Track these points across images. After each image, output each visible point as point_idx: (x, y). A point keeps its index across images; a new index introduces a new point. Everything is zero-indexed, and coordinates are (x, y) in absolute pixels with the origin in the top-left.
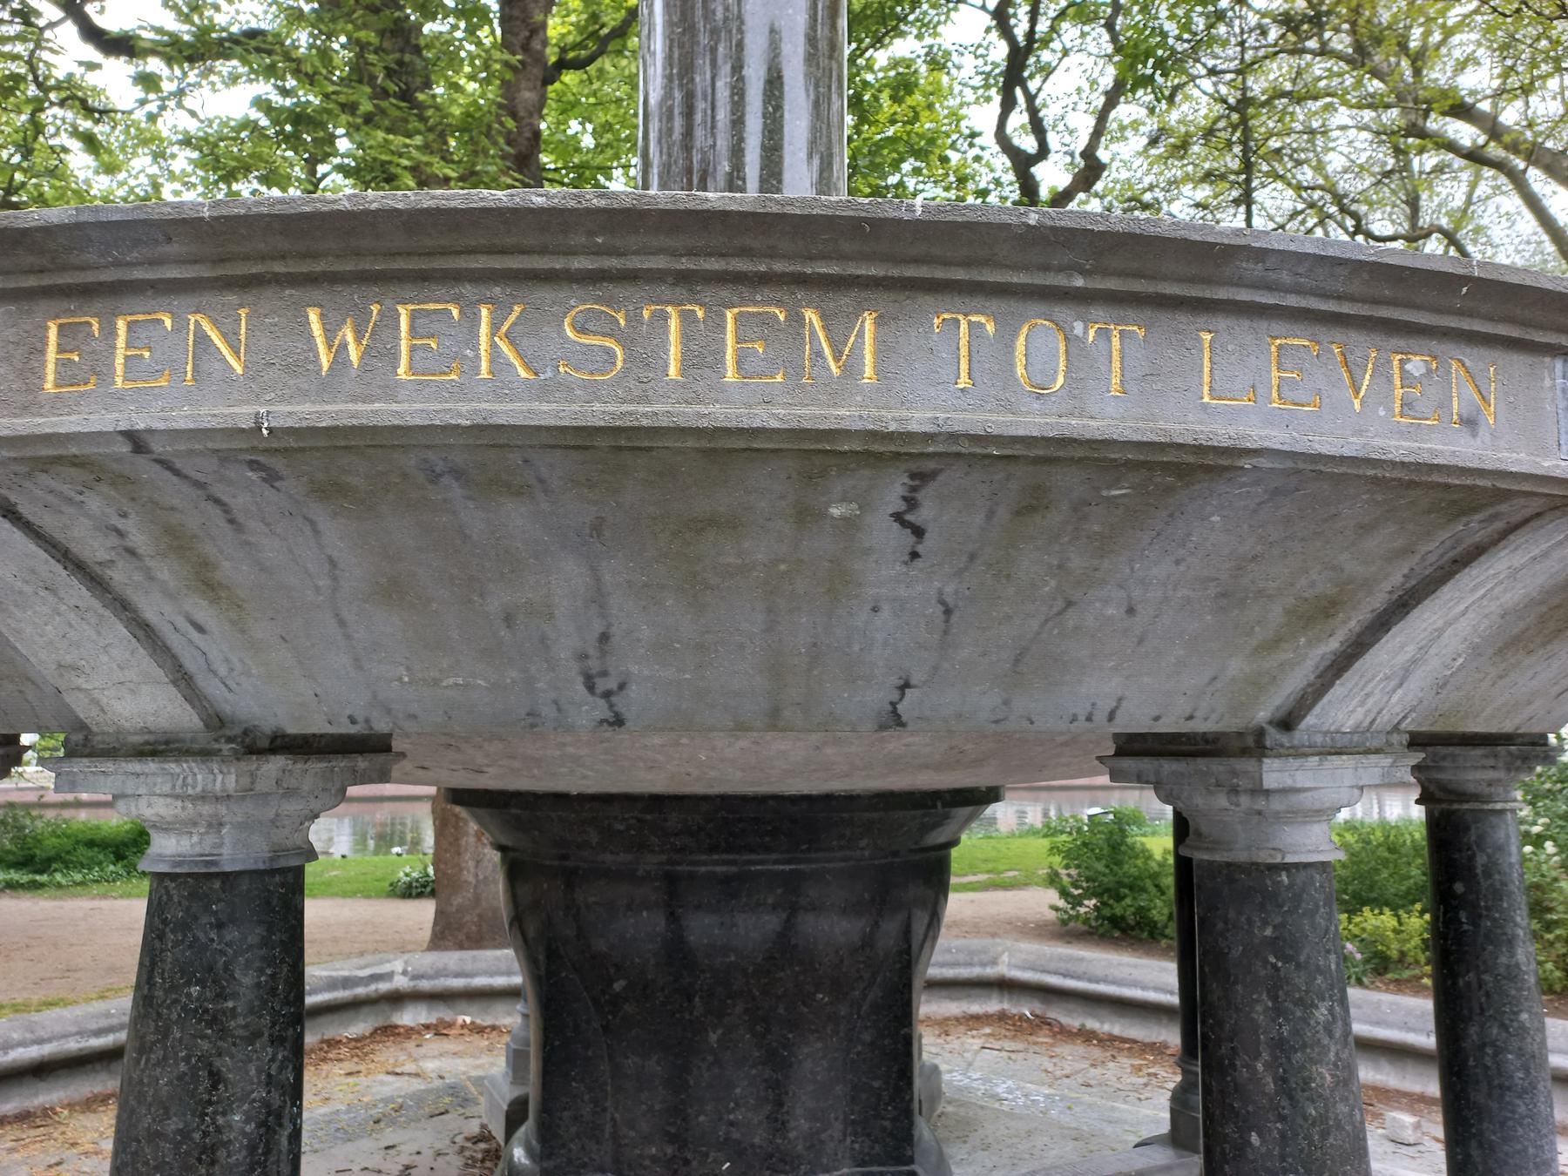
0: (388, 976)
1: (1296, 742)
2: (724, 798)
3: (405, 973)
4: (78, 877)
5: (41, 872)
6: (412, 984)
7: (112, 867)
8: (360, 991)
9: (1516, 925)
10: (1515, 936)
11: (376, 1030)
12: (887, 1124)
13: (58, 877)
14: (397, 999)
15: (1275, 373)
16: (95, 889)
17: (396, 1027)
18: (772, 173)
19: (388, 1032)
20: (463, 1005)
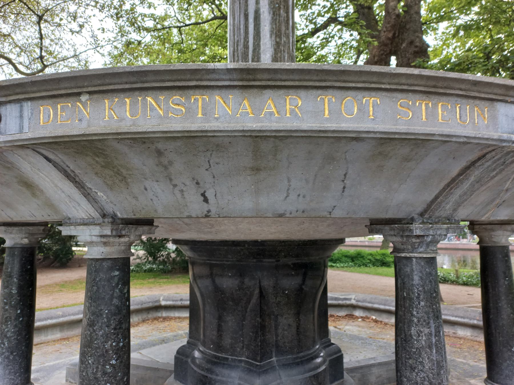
0: (350, 299)
1: (71, 222)
2: (255, 243)
3: (354, 299)
4: (342, 265)
5: (334, 263)
6: (356, 303)
7: (351, 264)
8: (340, 302)
9: (412, 315)
10: (412, 321)
11: (346, 315)
12: (253, 347)
13: (338, 265)
14: (354, 307)
15: (288, 107)
16: (345, 269)
17: (353, 315)
18: (257, 57)
19: (351, 317)
20: (373, 313)
